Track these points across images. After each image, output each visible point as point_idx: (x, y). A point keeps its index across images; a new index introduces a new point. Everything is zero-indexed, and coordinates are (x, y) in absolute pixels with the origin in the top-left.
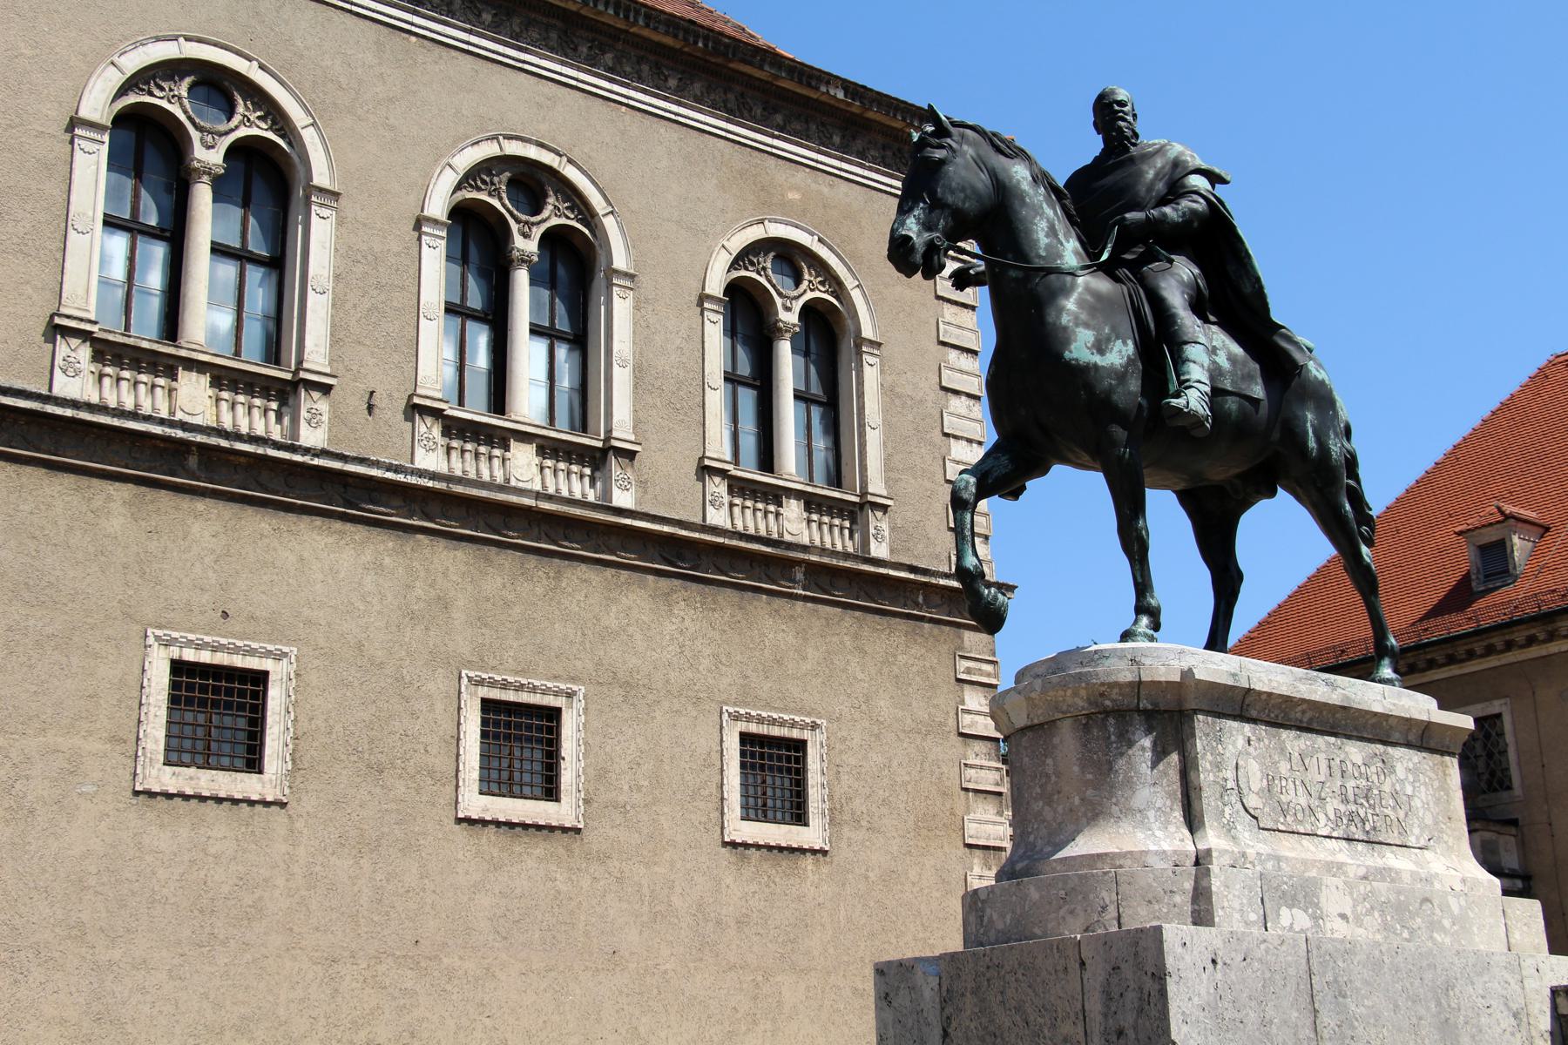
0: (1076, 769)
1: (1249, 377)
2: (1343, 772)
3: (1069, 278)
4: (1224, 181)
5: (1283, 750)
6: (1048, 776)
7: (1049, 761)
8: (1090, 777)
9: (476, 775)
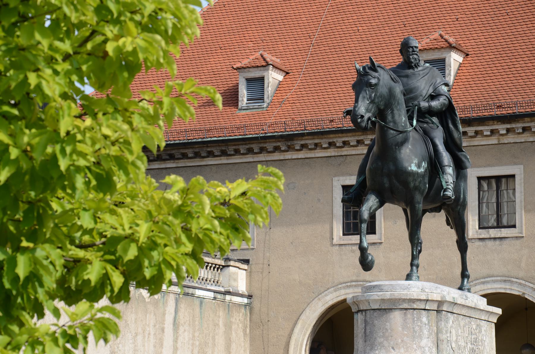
0: (400, 329)
5: (460, 324)
6: (386, 329)
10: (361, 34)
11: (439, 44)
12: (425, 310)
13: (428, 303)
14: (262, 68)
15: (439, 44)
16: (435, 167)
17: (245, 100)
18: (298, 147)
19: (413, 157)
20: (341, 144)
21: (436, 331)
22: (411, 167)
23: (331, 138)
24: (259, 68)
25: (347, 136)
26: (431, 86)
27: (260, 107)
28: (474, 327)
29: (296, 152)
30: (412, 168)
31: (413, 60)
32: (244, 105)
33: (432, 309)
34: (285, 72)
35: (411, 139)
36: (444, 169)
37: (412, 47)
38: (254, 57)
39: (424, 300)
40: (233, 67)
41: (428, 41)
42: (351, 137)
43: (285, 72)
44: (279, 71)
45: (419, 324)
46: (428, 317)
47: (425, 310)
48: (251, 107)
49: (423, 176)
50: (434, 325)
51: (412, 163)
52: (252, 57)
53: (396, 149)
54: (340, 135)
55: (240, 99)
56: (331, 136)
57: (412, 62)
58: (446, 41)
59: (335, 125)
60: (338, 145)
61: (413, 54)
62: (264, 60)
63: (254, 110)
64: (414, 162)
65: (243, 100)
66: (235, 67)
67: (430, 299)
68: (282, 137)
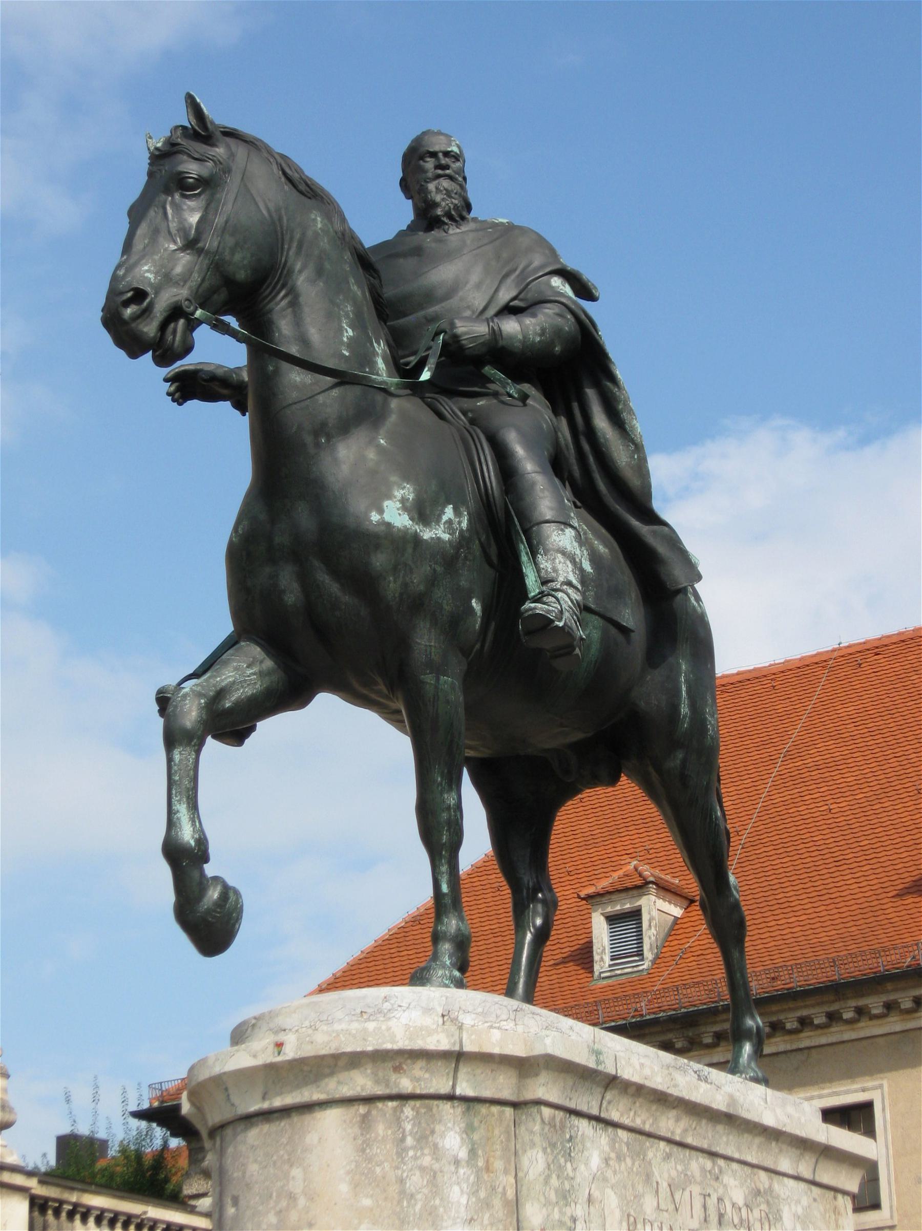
0: (344, 1188)
1: (616, 593)
2: (721, 1216)
3: (379, 397)
4: (591, 298)
5: (648, 1177)
6: (292, 1197)
7: (296, 1172)
8: (367, 1202)
9: (618, 1214)
10: (836, 816)
12: (450, 1097)
13: (464, 1071)
14: (635, 892)
16: (504, 531)
17: (607, 958)
18: (708, 1040)
19: (394, 478)
20: (795, 1025)
21: (511, 1194)
22: (381, 511)
23: (773, 1013)
24: (631, 893)
25: (806, 1007)
26: (506, 276)
27: (635, 969)
28: (738, 1195)
29: (706, 1051)
30: (387, 517)
31: (438, 198)
32: (606, 968)
33: (487, 1094)
34: (686, 898)
35: (393, 418)
37: (434, 155)
38: (621, 873)
39: (445, 1055)
40: (579, 897)
42: (813, 1006)
43: (686, 898)
44: (674, 898)
45: (427, 1160)
46: (469, 1129)
47: (450, 1097)
48: (619, 972)
49: (449, 558)
50: (498, 1165)
51: (389, 497)
52: (615, 875)
53: (318, 445)
54: (791, 1005)
55: (596, 957)
56: (774, 1008)
57: (435, 205)
59: (779, 984)
60: (789, 1026)
61: (438, 177)
62: (640, 875)
63: (623, 977)
64: (398, 494)
65: (602, 959)
66: (582, 895)
67: (468, 1048)
68: (672, 1020)
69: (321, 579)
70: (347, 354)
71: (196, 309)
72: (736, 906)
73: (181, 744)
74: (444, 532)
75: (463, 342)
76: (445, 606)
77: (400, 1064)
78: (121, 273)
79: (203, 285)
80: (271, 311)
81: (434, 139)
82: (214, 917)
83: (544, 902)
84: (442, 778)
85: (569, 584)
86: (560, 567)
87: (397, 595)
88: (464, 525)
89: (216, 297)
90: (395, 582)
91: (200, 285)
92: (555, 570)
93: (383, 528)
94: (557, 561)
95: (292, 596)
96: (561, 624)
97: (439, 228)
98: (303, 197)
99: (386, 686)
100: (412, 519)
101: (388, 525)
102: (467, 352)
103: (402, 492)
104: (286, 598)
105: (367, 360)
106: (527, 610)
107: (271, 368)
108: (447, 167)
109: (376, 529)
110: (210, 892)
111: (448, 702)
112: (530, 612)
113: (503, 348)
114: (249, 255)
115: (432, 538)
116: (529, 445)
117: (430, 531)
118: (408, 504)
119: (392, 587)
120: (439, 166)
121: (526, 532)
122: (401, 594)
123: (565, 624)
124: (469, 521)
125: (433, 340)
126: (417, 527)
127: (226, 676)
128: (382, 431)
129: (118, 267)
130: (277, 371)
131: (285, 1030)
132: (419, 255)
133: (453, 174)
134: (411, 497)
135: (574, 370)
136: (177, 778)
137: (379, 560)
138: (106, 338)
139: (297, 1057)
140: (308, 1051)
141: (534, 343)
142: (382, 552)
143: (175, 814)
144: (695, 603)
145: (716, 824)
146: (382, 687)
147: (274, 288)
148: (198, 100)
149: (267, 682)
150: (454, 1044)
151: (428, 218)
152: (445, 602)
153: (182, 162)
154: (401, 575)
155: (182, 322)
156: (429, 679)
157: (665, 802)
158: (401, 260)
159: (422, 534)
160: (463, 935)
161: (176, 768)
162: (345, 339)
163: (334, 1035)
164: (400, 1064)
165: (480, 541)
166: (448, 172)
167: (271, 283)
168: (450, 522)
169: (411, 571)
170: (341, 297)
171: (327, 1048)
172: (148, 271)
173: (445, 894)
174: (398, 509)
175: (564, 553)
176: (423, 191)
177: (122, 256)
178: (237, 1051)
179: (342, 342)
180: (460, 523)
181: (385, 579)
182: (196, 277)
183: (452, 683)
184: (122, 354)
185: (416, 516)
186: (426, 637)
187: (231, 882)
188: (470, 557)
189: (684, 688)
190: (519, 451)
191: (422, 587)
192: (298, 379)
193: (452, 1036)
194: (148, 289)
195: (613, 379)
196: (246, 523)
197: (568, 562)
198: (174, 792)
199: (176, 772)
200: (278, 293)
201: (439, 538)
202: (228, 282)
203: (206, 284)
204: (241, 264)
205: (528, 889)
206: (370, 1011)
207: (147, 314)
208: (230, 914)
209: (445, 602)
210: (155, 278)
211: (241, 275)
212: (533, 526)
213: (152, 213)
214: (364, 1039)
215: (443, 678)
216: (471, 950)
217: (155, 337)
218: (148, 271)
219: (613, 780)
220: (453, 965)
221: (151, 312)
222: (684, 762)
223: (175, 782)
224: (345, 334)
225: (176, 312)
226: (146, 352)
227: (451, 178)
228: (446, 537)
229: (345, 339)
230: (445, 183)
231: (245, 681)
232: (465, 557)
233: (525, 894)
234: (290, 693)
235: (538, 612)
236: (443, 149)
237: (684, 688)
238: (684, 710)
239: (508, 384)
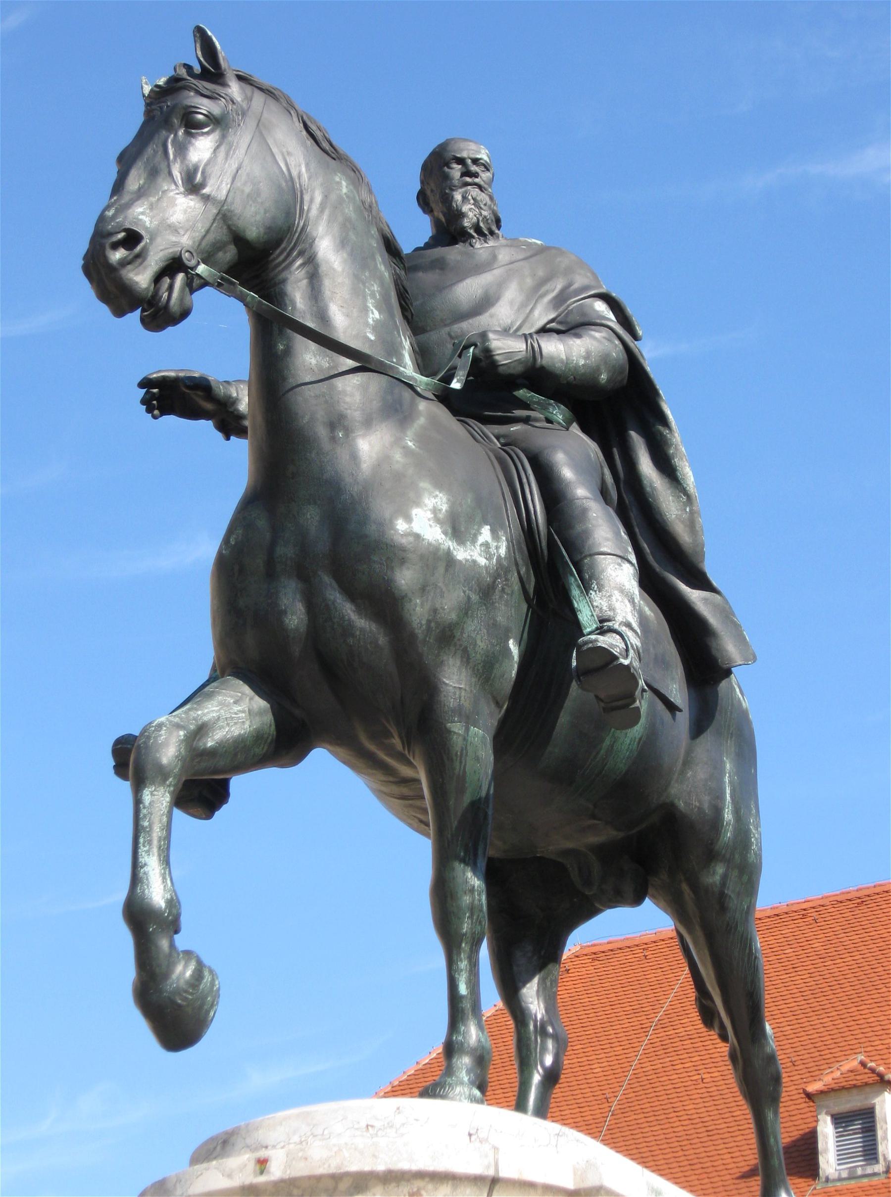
3: (407, 394)
11: (858, 1077)
15: (858, 1077)
16: (551, 565)
19: (424, 485)
22: (408, 519)
35: (422, 421)
36: (592, 566)
37: (461, 161)
39: (476, 1180)
41: (837, 1074)
49: (487, 590)
53: (333, 439)
58: (873, 1071)
61: (467, 184)
69: (332, 597)
70: (372, 338)
71: (198, 264)
72: (771, 1059)
73: (153, 783)
74: (481, 555)
75: (497, 358)
76: (479, 642)
77: (419, 1190)
78: (110, 213)
79: (207, 238)
80: (284, 281)
81: (462, 145)
82: (186, 999)
83: (555, 1037)
84: (465, 853)
85: (629, 625)
86: (618, 605)
87: (424, 622)
88: (503, 551)
89: (220, 254)
90: (422, 605)
91: (205, 236)
92: (612, 608)
93: (411, 539)
94: (614, 598)
95: (296, 617)
96: (626, 662)
97: (464, 242)
98: (326, 156)
99: (401, 738)
100: (445, 533)
101: (417, 536)
102: (501, 369)
103: (433, 501)
104: (287, 621)
105: (394, 350)
106: (586, 643)
107: (281, 347)
108: (476, 175)
109: (404, 541)
110: (179, 968)
111: (477, 759)
112: (590, 645)
113: (542, 368)
114: (262, 211)
115: (467, 560)
116: (576, 467)
117: (466, 551)
118: (441, 516)
119: (418, 612)
120: (467, 173)
121: (577, 565)
122: (429, 622)
123: (631, 662)
124: (508, 548)
125: (460, 356)
126: (450, 543)
127: (209, 710)
128: (410, 433)
129: (108, 208)
130: (288, 351)
131: (266, 1147)
132: (442, 269)
133: (482, 183)
134: (444, 507)
135: (621, 408)
136: (146, 824)
137: (405, 578)
138: (86, 290)
139: (286, 1177)
140: (301, 1170)
141: (576, 368)
142: (408, 569)
143: (142, 867)
144: (740, 696)
145: (756, 957)
146: (397, 742)
147: (289, 255)
148: (210, 33)
149: (257, 723)
150: (488, 1167)
151: (450, 231)
152: (479, 637)
153: (188, 97)
154: (430, 598)
155: (180, 277)
156: (457, 727)
157: (698, 928)
158: (420, 274)
159: (455, 553)
160: (483, 1048)
161: (144, 811)
162: (370, 321)
163: (335, 1149)
164: (419, 1190)
165: (519, 573)
166: (477, 180)
167: (285, 249)
168: (486, 545)
169: (442, 596)
170: (367, 274)
171: (326, 1166)
172: (143, 213)
173: (462, 997)
174: (429, 520)
175: (622, 591)
176: (447, 200)
177: (112, 196)
178: (207, 1169)
179: (367, 324)
180: (497, 548)
181: (410, 600)
182: (201, 228)
183: (484, 737)
184: (104, 310)
185: (450, 531)
186: (455, 677)
187: (206, 961)
188: (508, 590)
189: (728, 791)
190: (567, 473)
191: (453, 616)
192: (313, 361)
193: (486, 1156)
194: (143, 233)
195: (663, 420)
196: (240, 531)
197: (627, 602)
198: (141, 840)
199: (145, 816)
200: (294, 261)
201: (474, 562)
202: (238, 239)
203: (211, 237)
204: (254, 220)
205: (535, 1021)
206: (378, 1124)
207: (139, 260)
208: (203, 998)
209: (479, 637)
210: (151, 222)
211: (253, 232)
212: (585, 557)
213: (149, 151)
214: (374, 1156)
215: (473, 730)
216: (490, 1072)
217: (147, 289)
218: (143, 213)
219: (637, 901)
220: (472, 1083)
221: (144, 260)
222: (725, 877)
223: (144, 828)
224: (371, 315)
225: (174, 266)
226: (132, 310)
227: (480, 187)
228: (482, 561)
229: (370, 321)
230: (474, 192)
231: (232, 718)
232: (503, 589)
233: (532, 1027)
234: (284, 743)
235: (599, 644)
236: (473, 156)
237: (728, 791)
238: (728, 815)
239: (551, 405)
